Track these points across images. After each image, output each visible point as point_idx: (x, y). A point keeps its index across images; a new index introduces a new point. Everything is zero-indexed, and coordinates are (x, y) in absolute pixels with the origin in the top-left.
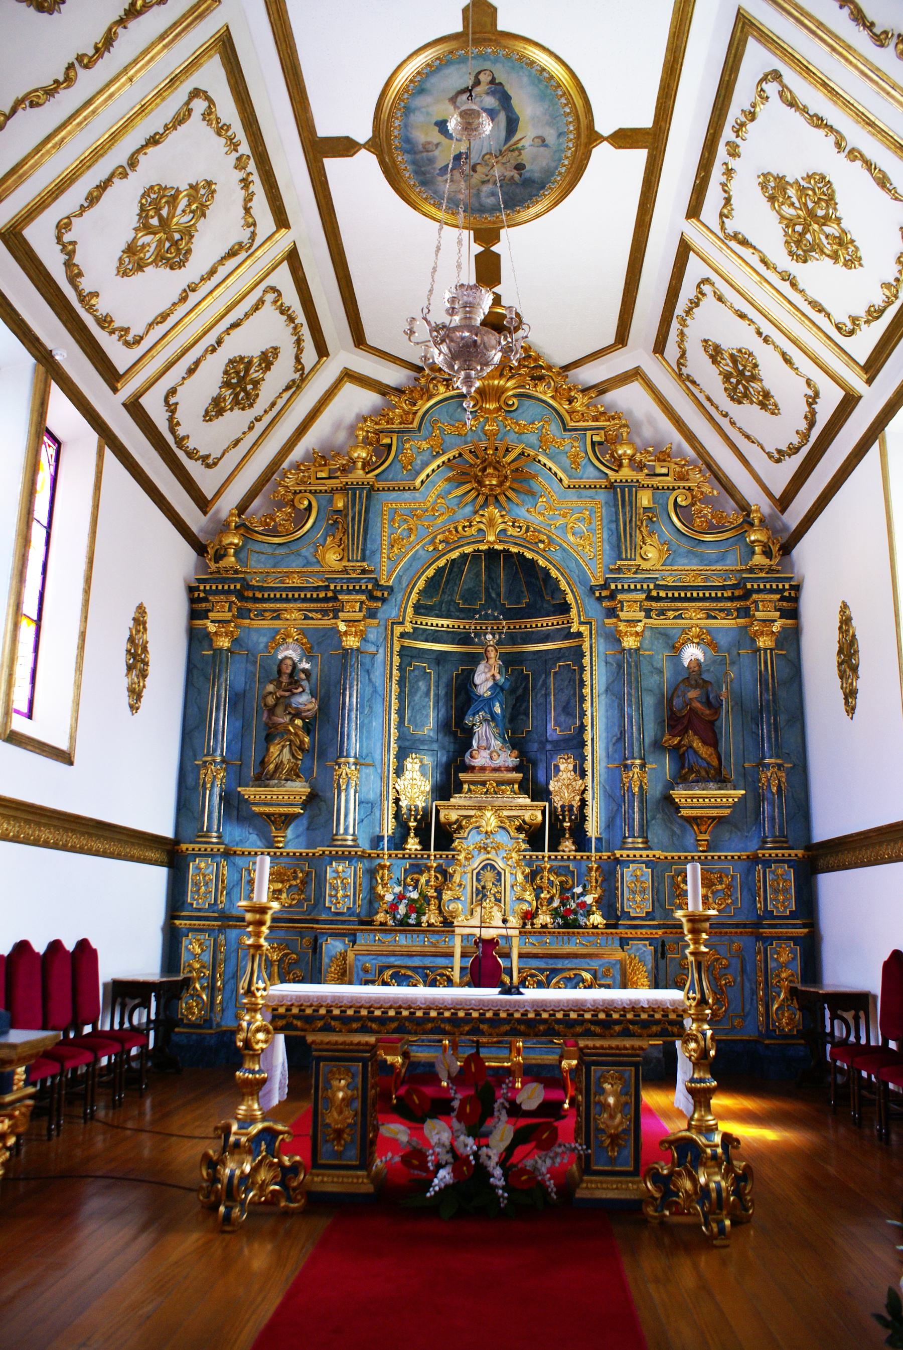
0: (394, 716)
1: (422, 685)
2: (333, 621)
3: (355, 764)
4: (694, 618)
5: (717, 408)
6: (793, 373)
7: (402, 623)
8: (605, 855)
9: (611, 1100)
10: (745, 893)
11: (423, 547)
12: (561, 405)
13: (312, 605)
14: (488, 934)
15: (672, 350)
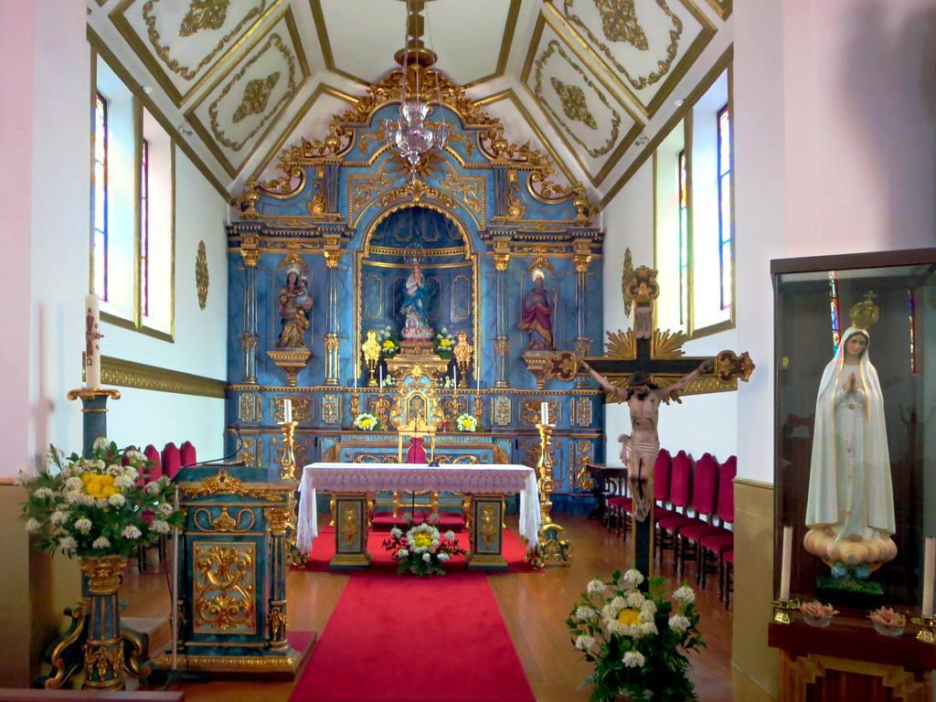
0: (360, 309)
1: (374, 288)
2: (320, 250)
3: (337, 337)
4: (540, 253)
5: (559, 120)
6: (605, 107)
7: (363, 252)
8: (484, 391)
9: (488, 519)
10: (564, 414)
11: (375, 204)
12: (461, 112)
13: (307, 240)
14: (419, 435)
15: (532, 82)
